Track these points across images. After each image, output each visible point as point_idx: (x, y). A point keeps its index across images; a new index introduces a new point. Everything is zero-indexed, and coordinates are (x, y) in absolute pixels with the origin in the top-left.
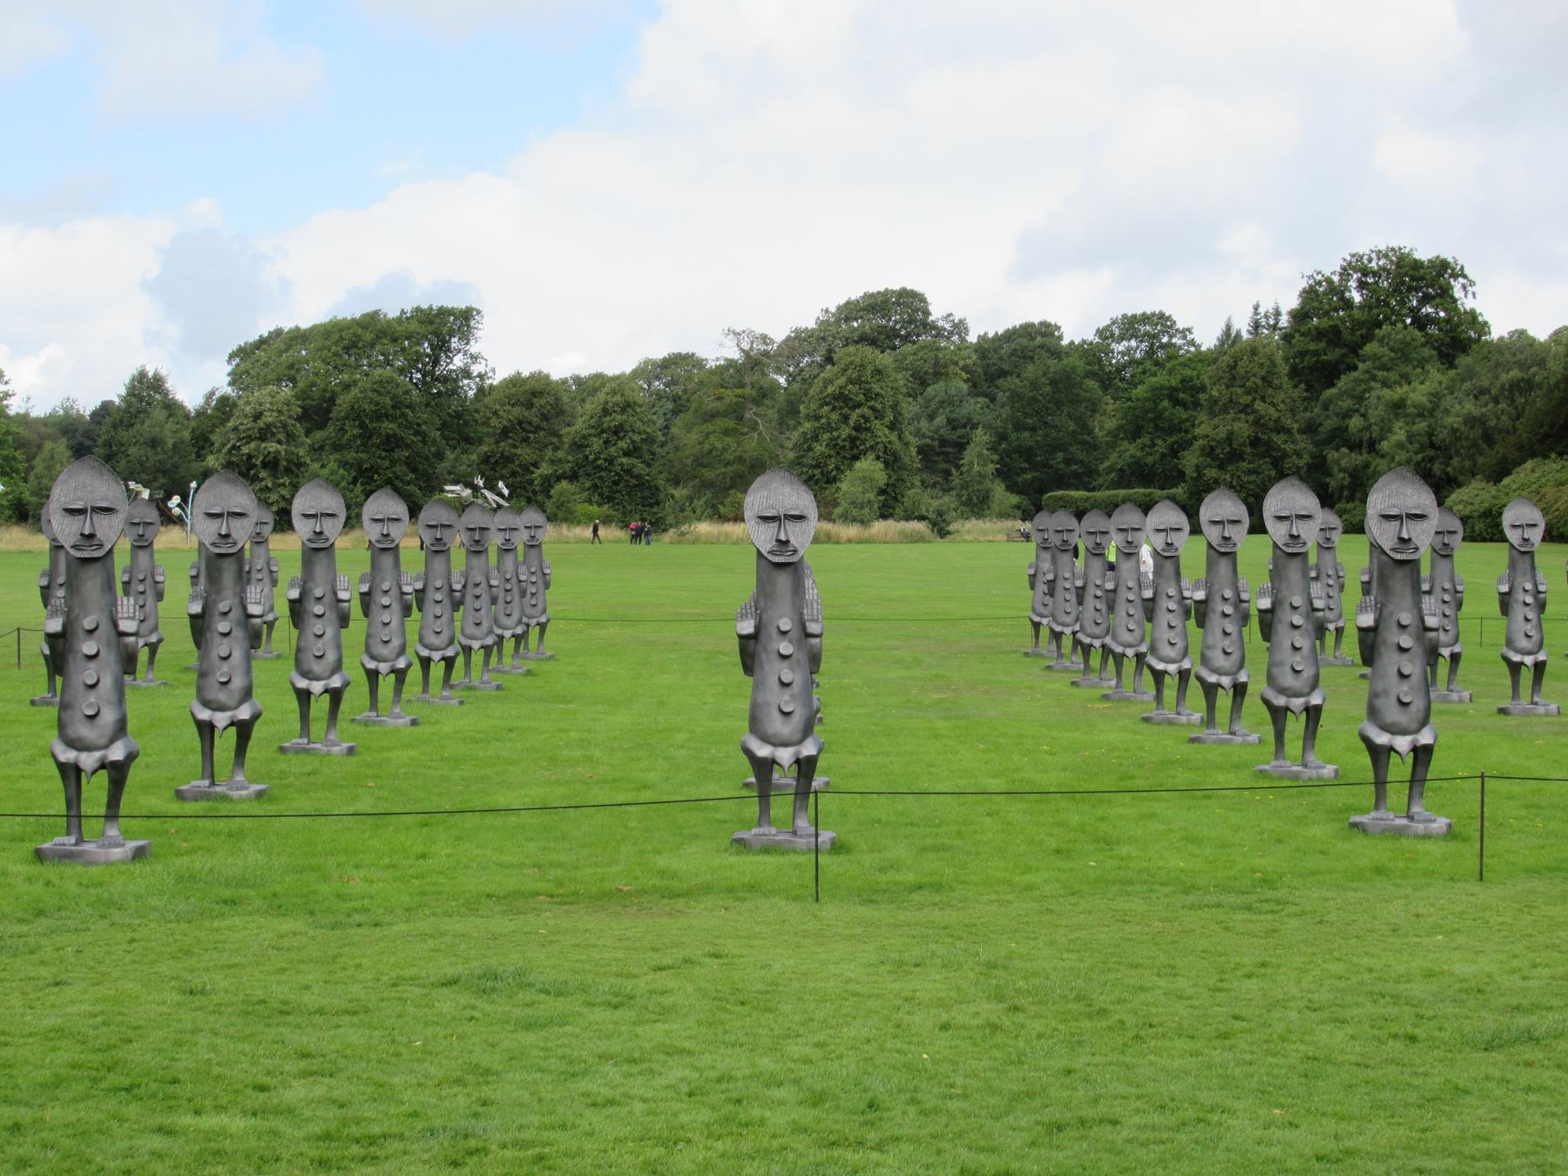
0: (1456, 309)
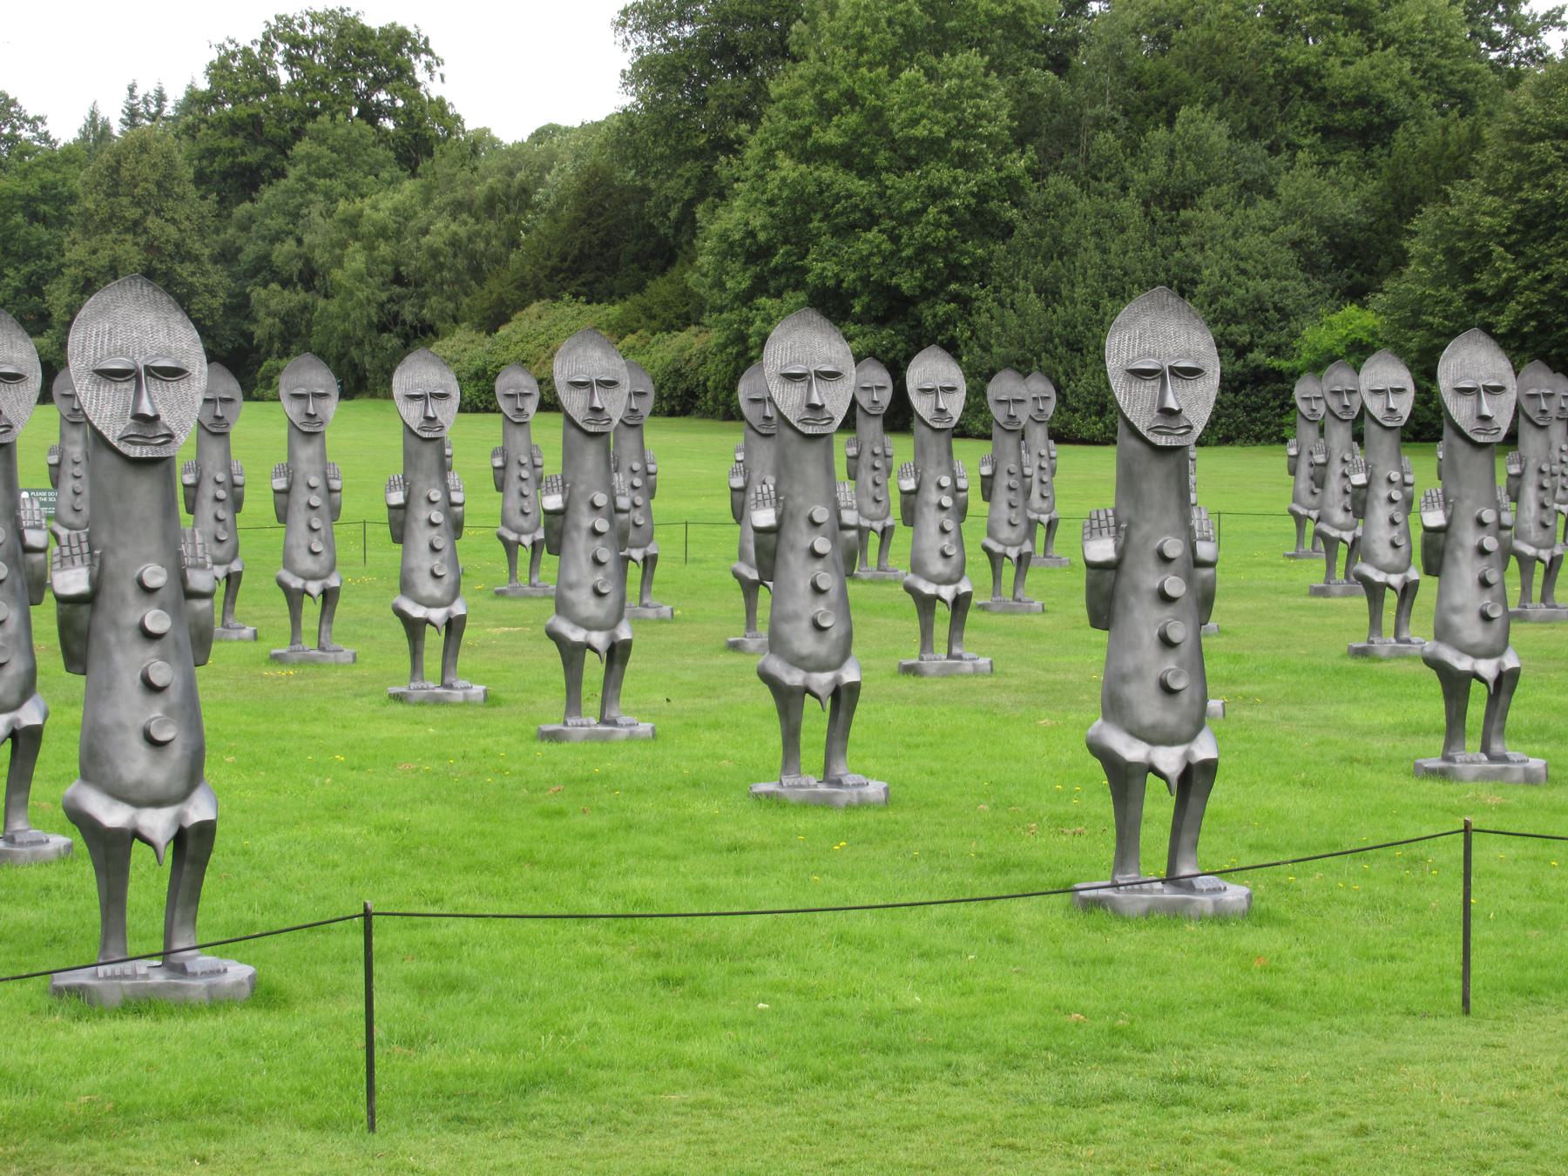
0: (419, 97)
